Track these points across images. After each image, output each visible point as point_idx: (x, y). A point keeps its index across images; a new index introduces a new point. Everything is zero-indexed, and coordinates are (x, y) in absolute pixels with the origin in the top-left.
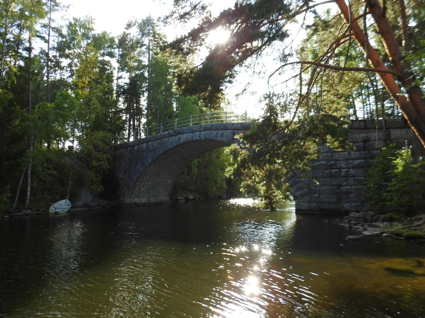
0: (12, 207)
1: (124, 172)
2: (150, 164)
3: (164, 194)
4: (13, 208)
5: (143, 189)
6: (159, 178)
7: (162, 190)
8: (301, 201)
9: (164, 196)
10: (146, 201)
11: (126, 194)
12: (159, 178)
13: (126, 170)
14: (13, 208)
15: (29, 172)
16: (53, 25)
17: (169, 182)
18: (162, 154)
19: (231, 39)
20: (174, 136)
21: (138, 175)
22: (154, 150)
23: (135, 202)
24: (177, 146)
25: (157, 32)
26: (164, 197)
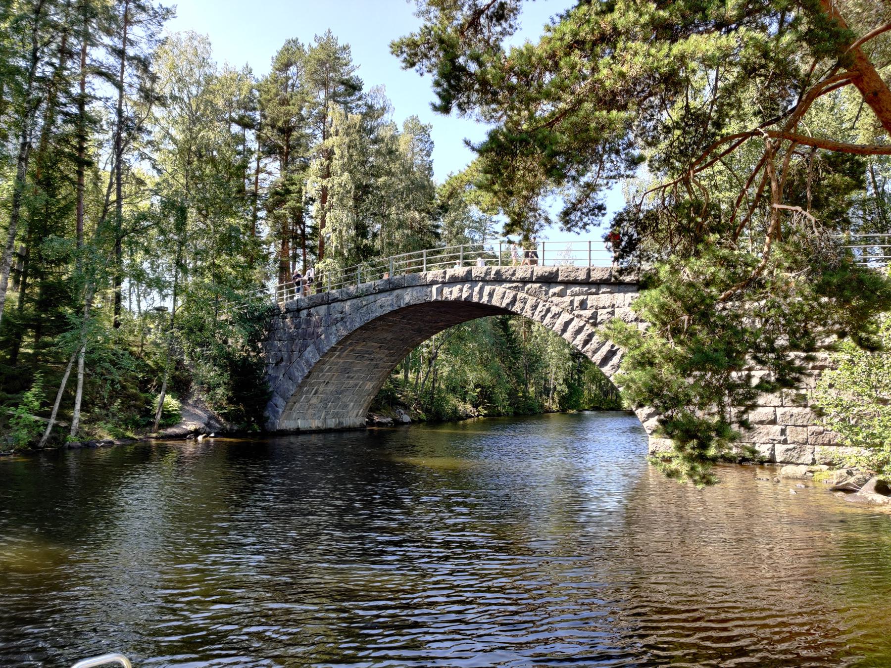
0: (41, 435)
1: (277, 364)
2: (333, 349)
3: (355, 412)
4: (45, 438)
5: (314, 401)
6: (348, 377)
7: (352, 404)
8: (473, 494)
9: (357, 415)
10: (320, 425)
11: (281, 411)
12: (348, 377)
13: (282, 360)
14: (45, 438)
15: (81, 361)
16: (131, 51)
17: (369, 386)
18: (361, 328)
19: (589, 419)
20: (387, 291)
21: (306, 371)
22: (342, 319)
23: (298, 429)
24: (393, 313)
25: (483, 275)
26: (354, 417)
